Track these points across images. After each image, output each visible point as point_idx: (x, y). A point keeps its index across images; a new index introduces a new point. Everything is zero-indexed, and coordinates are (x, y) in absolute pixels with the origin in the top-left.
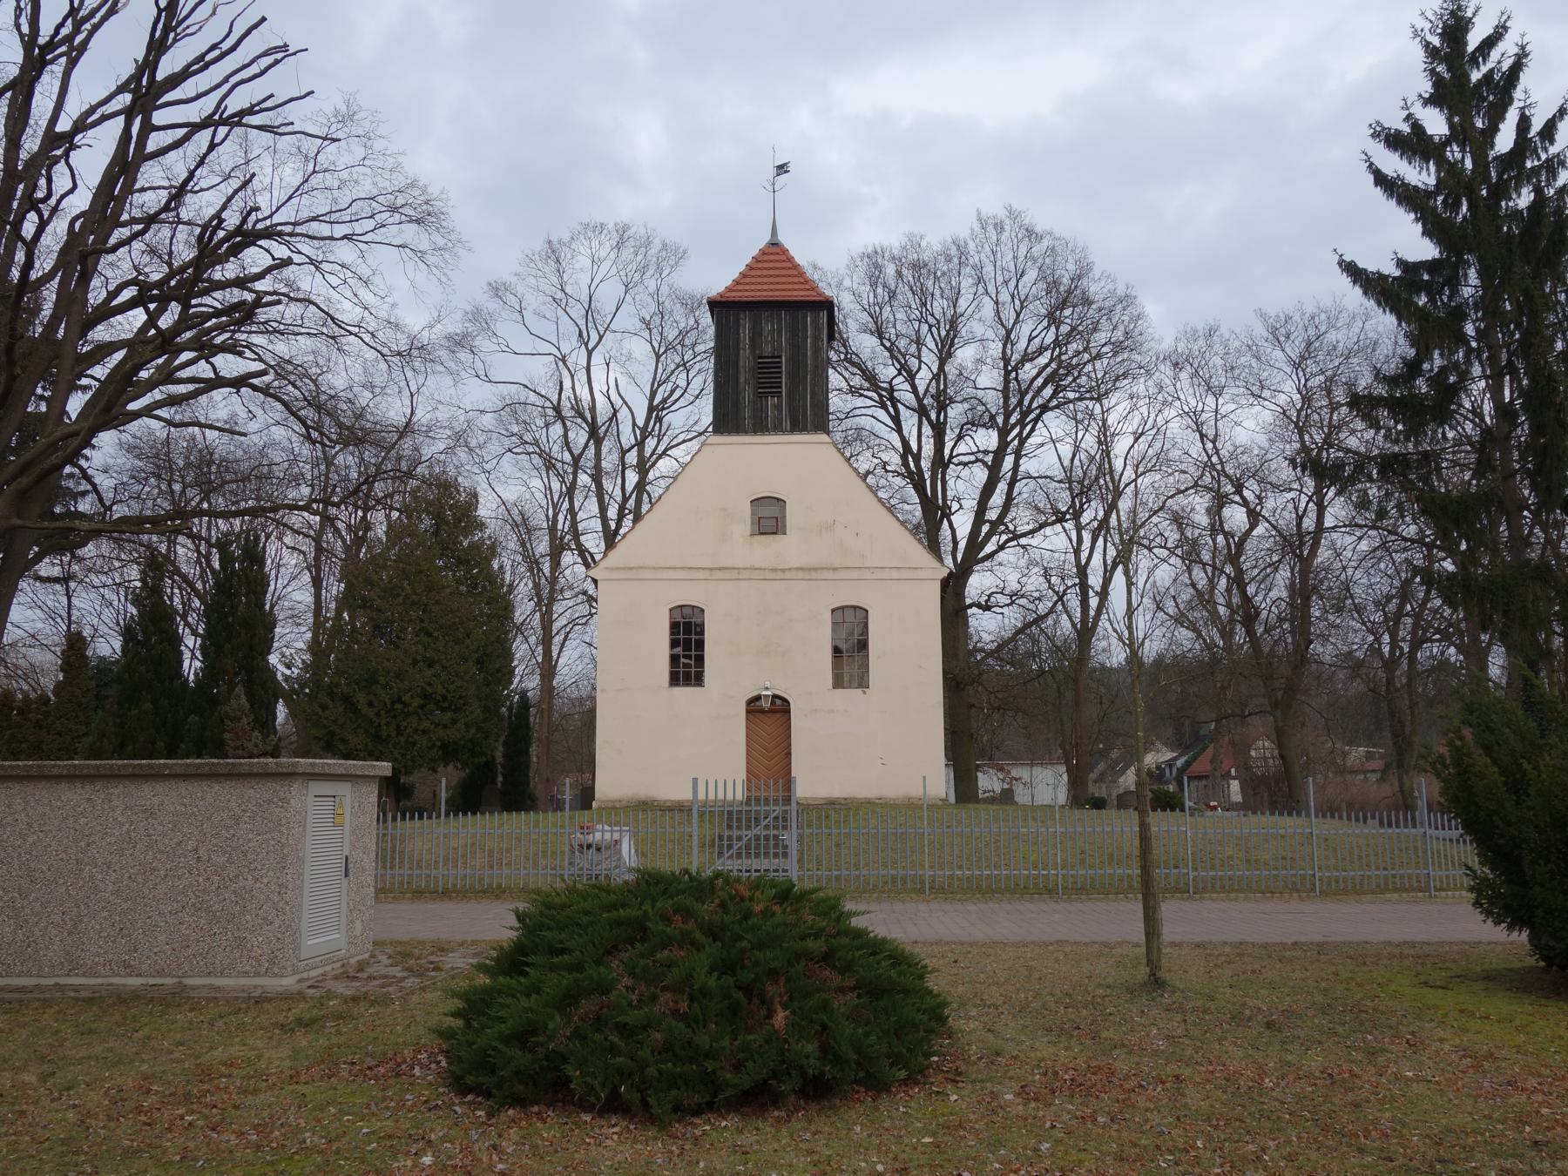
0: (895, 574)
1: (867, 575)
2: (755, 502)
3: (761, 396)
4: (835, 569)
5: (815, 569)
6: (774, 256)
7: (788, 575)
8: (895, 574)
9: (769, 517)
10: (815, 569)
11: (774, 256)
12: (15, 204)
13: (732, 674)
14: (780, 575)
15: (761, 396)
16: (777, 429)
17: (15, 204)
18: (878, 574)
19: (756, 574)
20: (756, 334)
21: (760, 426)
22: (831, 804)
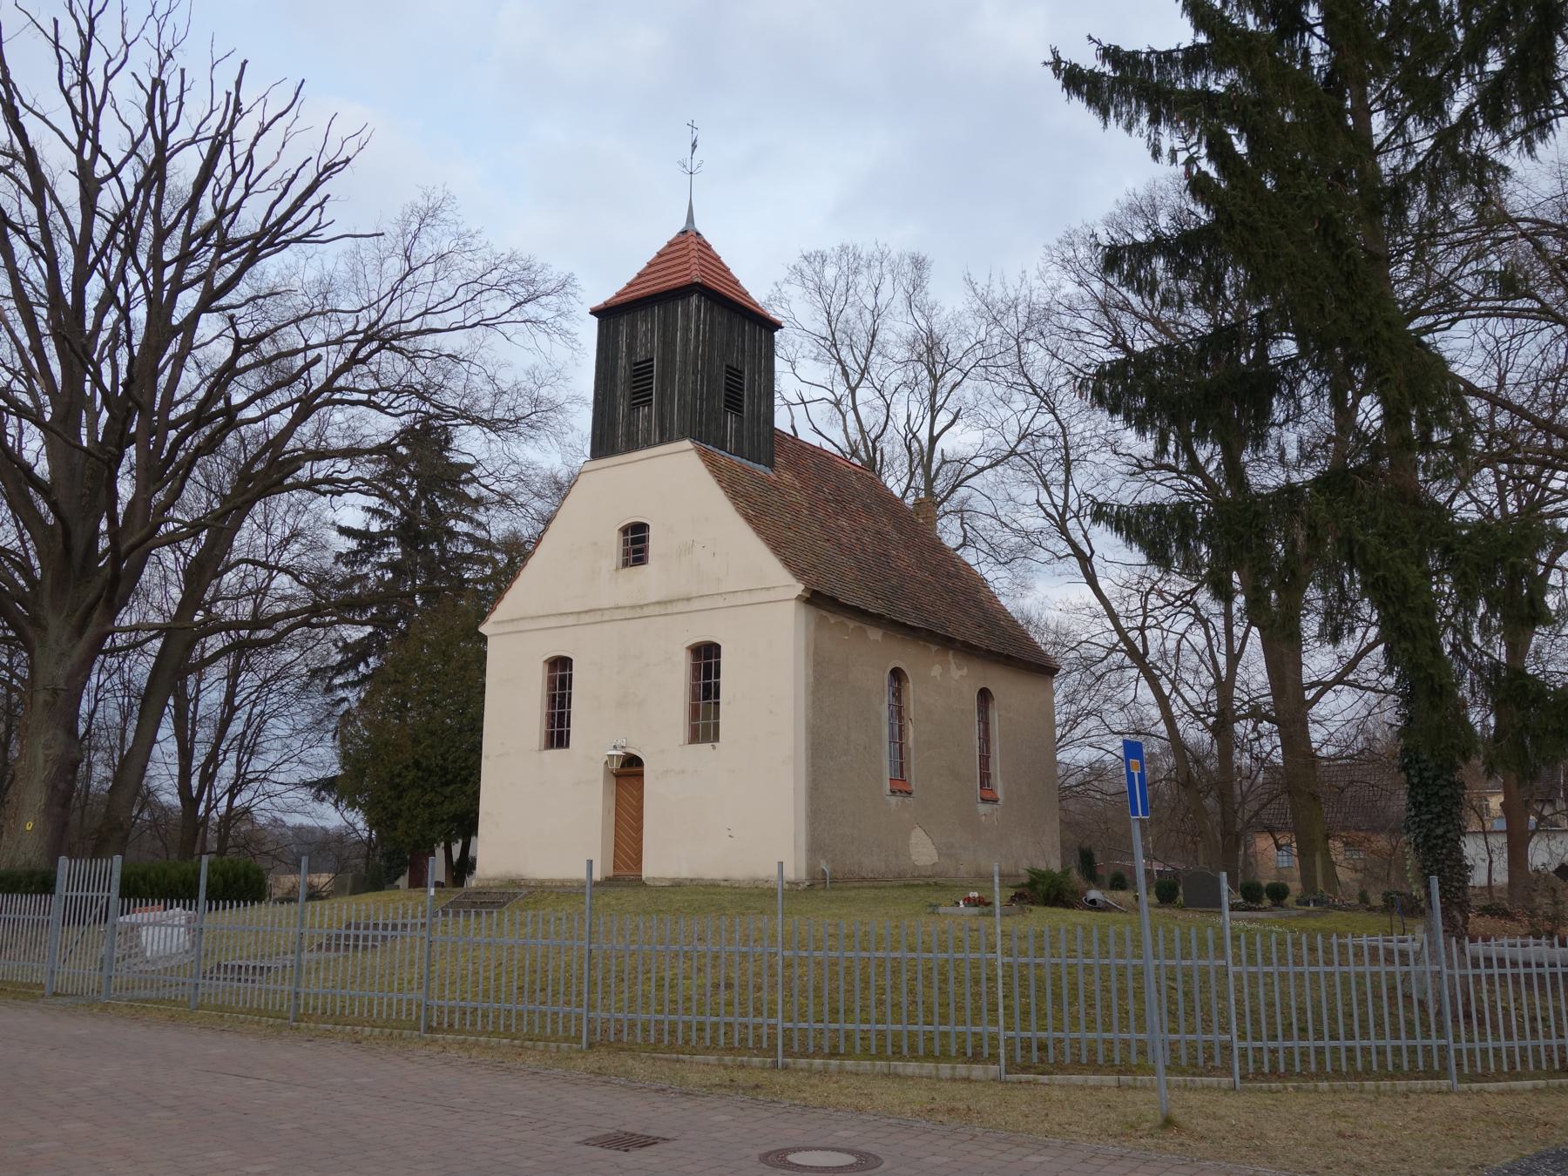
0: (747, 598)
1: (720, 602)
2: (718, 647)
3: (634, 407)
4: (688, 599)
5: (671, 602)
6: (689, 243)
7: (646, 611)
8: (747, 598)
9: (635, 542)
10: (671, 602)
11: (689, 243)
12: (22, 582)
13: (596, 734)
14: (639, 613)
15: (634, 407)
16: (648, 444)
17: (22, 582)
18: (731, 601)
19: (618, 615)
20: (632, 337)
21: (632, 445)
22: (677, 885)
